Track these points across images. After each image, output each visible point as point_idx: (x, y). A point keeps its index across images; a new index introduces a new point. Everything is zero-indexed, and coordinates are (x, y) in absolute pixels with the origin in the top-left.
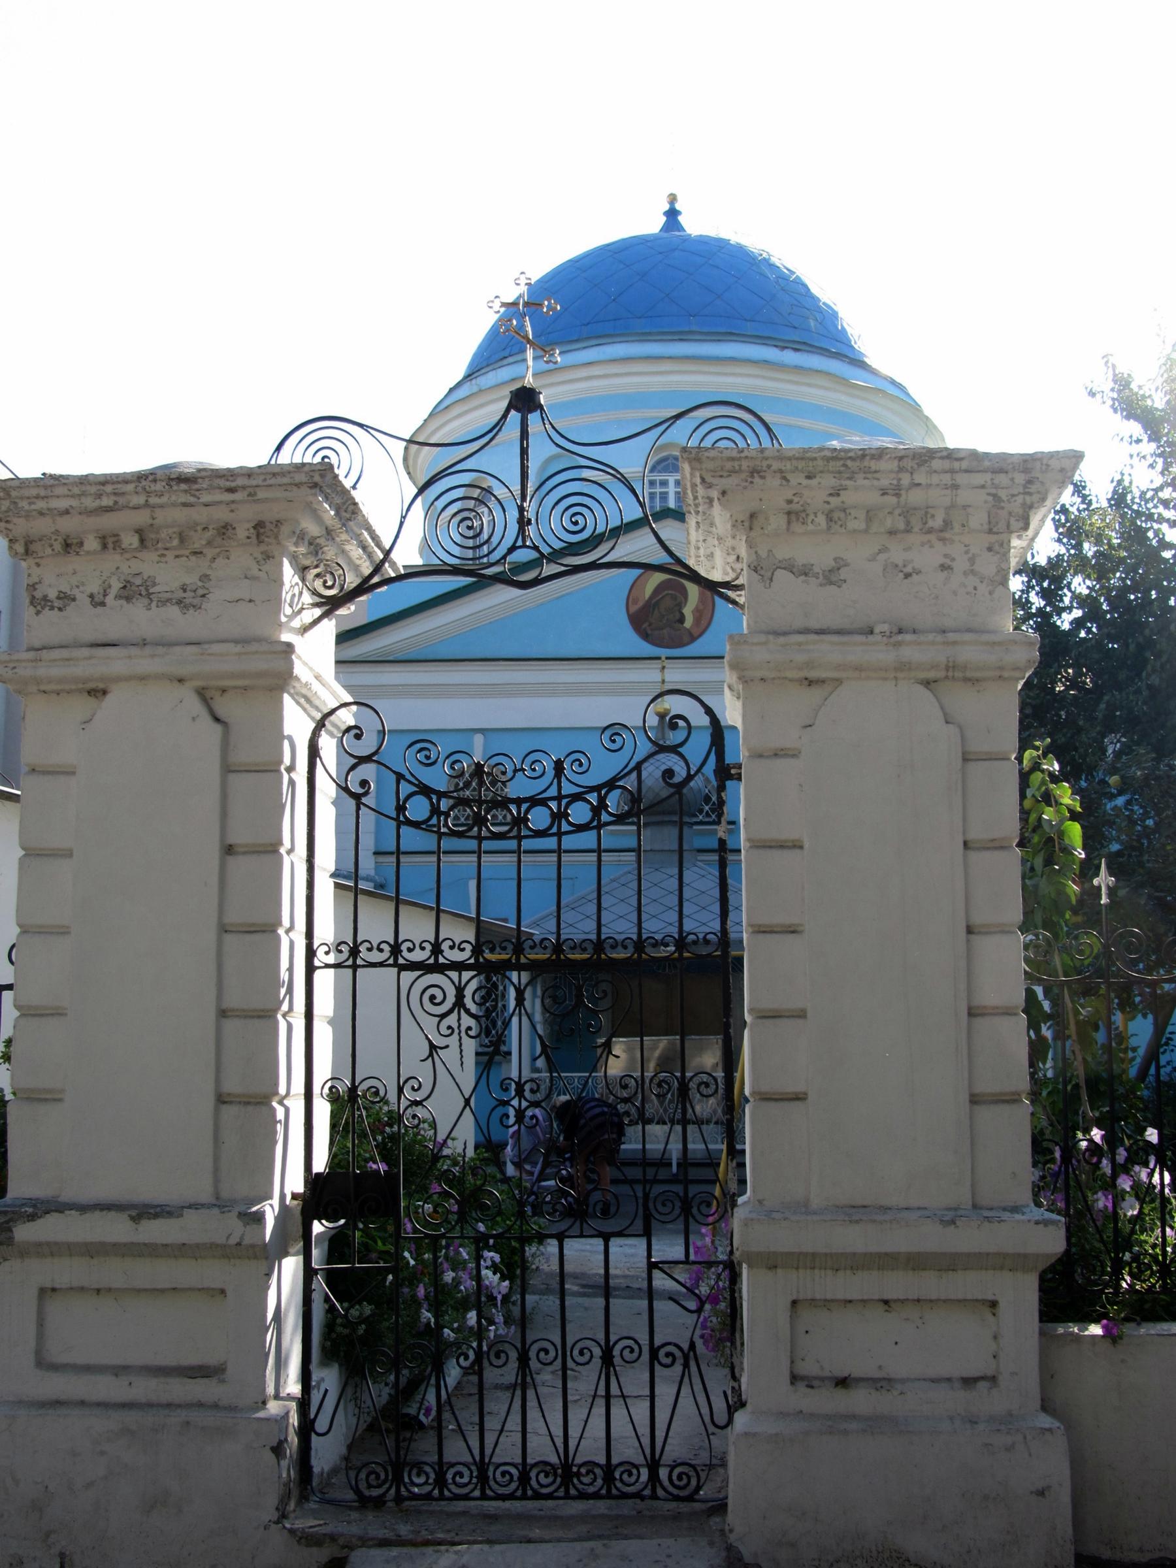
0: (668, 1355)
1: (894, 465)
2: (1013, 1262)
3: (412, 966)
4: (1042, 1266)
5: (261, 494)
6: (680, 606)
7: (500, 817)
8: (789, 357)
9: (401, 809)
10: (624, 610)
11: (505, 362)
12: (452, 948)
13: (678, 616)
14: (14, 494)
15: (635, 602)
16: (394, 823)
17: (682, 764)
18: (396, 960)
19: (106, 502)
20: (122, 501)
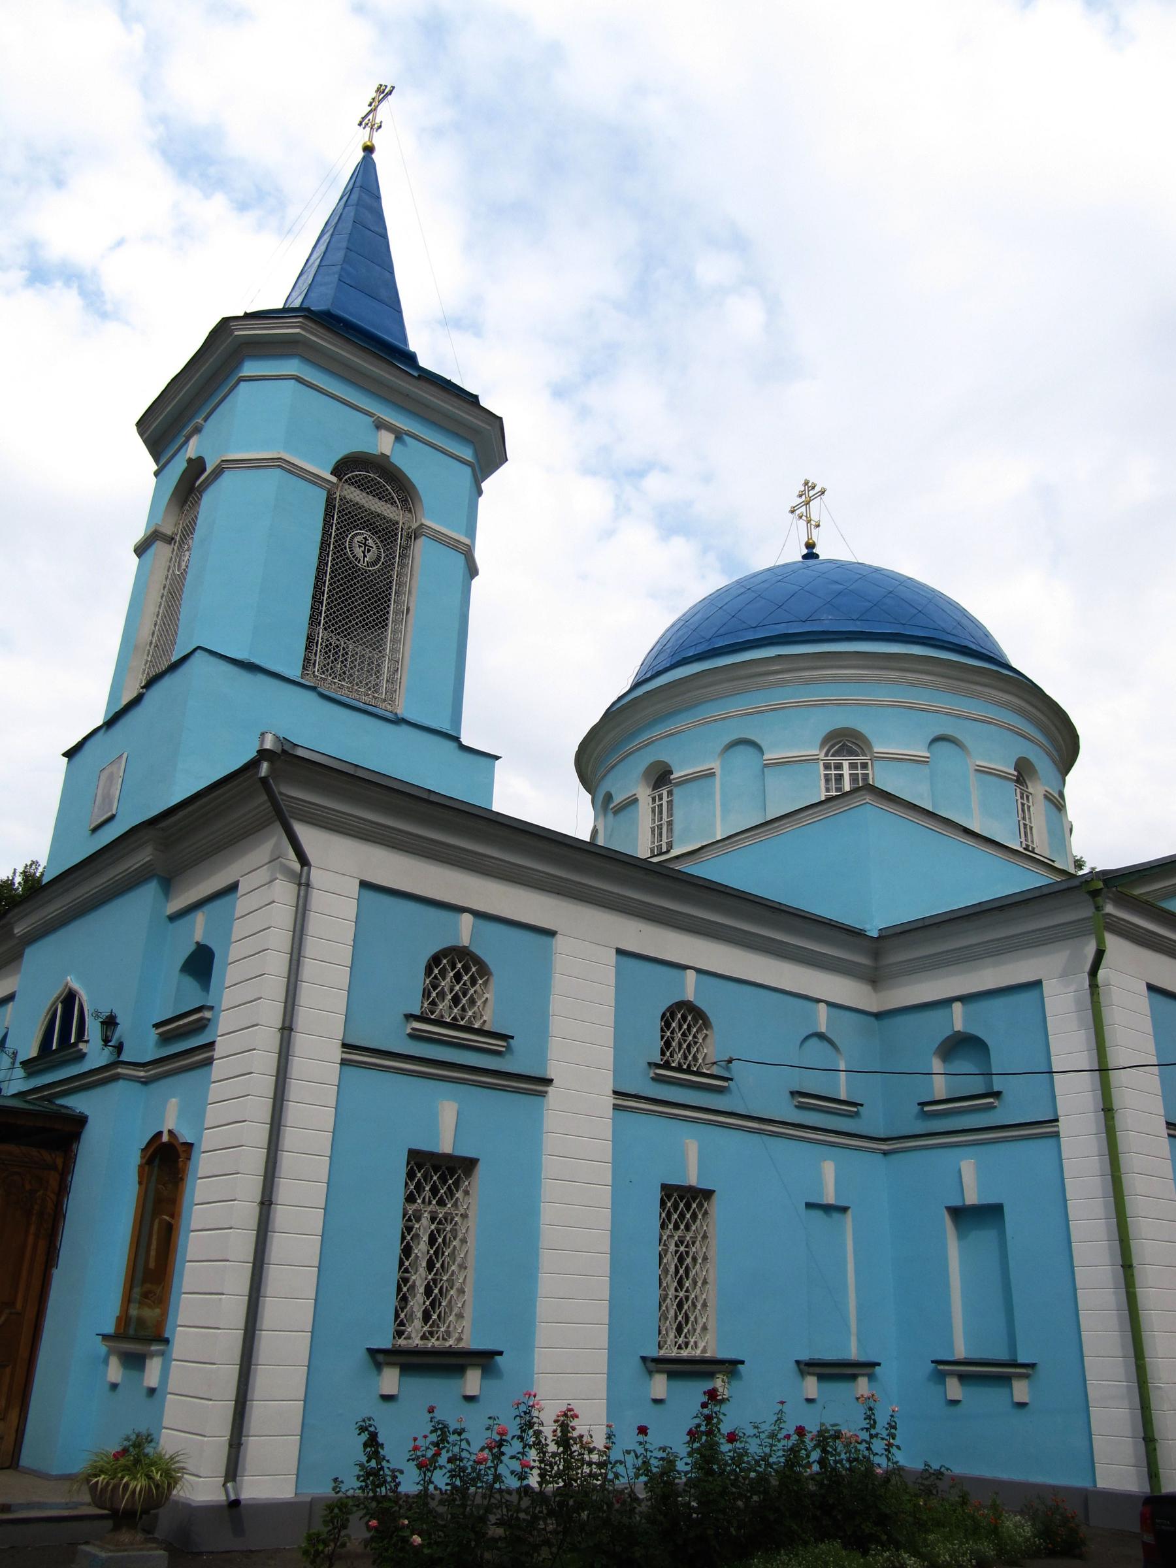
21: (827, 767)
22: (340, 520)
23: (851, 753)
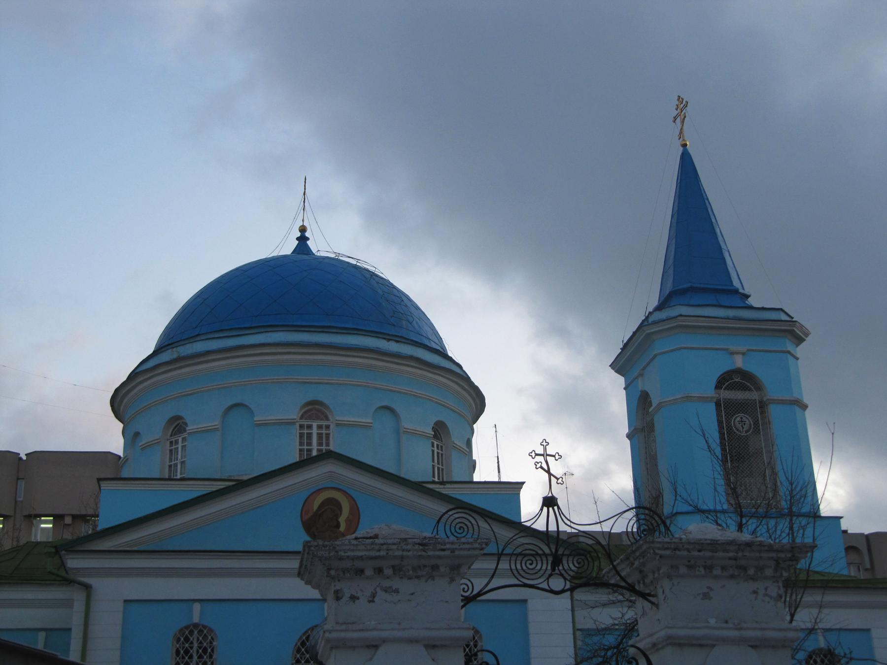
5: (457, 552)
6: (337, 516)
8: (393, 347)
10: (299, 518)
11: (198, 338)
14: (338, 548)
17: (493, 658)
19: (382, 553)
20: (390, 553)
21: (301, 427)
22: (726, 410)
23: (318, 418)
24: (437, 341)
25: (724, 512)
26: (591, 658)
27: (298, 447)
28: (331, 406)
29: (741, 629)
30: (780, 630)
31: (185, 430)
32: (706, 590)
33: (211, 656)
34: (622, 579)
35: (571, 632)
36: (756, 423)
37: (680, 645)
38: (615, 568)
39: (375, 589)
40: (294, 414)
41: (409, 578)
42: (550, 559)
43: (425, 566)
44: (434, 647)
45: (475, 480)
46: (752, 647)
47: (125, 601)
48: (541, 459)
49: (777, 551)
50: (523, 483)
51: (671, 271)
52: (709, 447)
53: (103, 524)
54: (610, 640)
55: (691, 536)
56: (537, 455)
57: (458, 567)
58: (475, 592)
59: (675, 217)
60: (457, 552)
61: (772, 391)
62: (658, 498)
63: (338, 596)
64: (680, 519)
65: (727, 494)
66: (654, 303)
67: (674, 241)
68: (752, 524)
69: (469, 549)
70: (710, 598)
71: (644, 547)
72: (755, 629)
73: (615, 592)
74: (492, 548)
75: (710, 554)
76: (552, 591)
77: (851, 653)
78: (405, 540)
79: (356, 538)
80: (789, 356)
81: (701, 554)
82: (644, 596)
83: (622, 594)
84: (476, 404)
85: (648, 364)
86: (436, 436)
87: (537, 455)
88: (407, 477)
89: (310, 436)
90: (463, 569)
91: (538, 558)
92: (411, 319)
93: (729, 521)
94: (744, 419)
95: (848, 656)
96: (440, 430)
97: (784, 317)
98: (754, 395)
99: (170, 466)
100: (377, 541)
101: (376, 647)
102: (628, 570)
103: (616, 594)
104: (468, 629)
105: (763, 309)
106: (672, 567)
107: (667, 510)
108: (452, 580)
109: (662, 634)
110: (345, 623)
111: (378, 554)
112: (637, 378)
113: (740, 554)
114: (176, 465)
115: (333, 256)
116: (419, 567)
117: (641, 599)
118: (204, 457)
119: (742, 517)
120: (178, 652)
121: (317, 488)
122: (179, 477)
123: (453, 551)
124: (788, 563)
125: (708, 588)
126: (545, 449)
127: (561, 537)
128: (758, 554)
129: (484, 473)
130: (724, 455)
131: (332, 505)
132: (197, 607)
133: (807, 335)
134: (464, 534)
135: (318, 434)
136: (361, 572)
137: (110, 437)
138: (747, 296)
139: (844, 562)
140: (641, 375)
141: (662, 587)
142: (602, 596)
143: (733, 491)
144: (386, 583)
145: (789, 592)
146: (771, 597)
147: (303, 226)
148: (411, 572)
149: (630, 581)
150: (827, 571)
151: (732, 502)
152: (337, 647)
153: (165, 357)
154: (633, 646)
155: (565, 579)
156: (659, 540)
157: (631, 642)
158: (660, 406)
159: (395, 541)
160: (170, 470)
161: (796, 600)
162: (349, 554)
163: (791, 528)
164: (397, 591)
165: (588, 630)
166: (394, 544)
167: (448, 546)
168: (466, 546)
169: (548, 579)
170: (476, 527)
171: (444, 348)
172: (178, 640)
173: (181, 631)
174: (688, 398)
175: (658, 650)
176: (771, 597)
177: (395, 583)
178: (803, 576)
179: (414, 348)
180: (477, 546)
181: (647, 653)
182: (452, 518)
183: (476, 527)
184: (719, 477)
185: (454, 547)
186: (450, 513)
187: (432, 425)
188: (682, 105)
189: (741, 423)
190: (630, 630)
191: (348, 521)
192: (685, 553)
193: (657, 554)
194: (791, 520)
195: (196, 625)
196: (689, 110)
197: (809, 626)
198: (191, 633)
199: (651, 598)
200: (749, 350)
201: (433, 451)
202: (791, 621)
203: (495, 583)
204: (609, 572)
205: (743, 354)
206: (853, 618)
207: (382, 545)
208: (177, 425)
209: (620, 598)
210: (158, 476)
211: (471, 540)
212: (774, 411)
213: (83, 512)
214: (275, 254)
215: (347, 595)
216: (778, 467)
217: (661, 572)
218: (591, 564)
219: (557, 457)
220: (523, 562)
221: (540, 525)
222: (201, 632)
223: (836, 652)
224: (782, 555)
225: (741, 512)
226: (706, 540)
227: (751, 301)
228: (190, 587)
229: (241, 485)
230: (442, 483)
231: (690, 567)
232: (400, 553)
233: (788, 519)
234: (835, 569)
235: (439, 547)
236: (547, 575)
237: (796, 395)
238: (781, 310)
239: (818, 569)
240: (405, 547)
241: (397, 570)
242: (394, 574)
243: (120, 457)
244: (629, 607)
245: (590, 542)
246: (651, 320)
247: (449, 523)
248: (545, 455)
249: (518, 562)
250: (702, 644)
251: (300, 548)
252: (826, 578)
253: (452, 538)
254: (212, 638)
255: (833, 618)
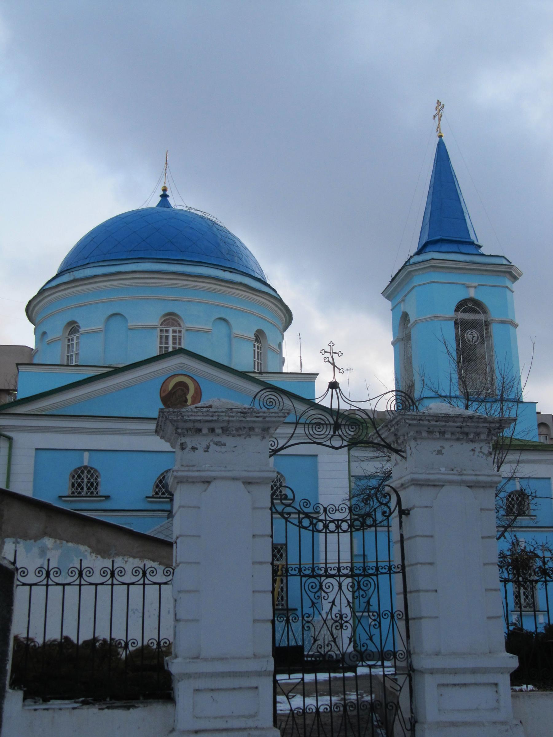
0: (391, 706)
1: (462, 420)
2: (500, 671)
3: (305, 576)
4: (511, 671)
5: (267, 419)
7: (95, 493)
8: (228, 276)
9: (300, 522)
11: (88, 266)
12: (331, 570)
13: (184, 399)
14: (183, 414)
15: (164, 391)
16: (298, 528)
17: (290, 491)
18: (300, 574)
19: (215, 418)
21: (161, 331)
22: (461, 326)
23: (173, 325)
24: (259, 273)
25: (456, 397)
26: (360, 495)
27: (159, 345)
28: (182, 317)
29: (462, 475)
30: (489, 476)
31: (78, 331)
32: (440, 448)
33: (96, 489)
34: (383, 440)
35: (348, 477)
36: (482, 336)
37: (421, 485)
38: (377, 432)
39: (209, 443)
40: (156, 322)
41: (233, 436)
42: (332, 426)
43: (244, 428)
44: (250, 483)
45: (284, 371)
46: (469, 487)
47: (37, 449)
48: (328, 355)
49: (490, 422)
50: (317, 374)
51: (427, 227)
52: (448, 351)
53: (20, 395)
54: (374, 483)
55: (431, 412)
56: (326, 352)
57: (268, 428)
58: (279, 447)
59: (432, 188)
60: (267, 419)
61: (494, 314)
62: (411, 387)
63: (183, 447)
64: (426, 402)
65: (459, 384)
66: (415, 250)
67: (430, 206)
68: (475, 405)
69: (276, 417)
70: (442, 454)
71: (398, 418)
72: (471, 475)
73: (378, 450)
74: (291, 418)
75: (443, 423)
76: (333, 447)
77: (535, 492)
78: (231, 409)
79: (196, 407)
80: (507, 290)
81: (438, 423)
82: (397, 452)
83: (383, 452)
84: (286, 318)
85: (408, 293)
86: (257, 340)
87: (326, 352)
88: (236, 368)
89: (167, 337)
90: (272, 431)
91: (325, 427)
92: (241, 256)
93: (460, 403)
94: (474, 333)
95: (533, 495)
96: (259, 336)
97: (505, 262)
98: (481, 317)
99: (68, 356)
100: (211, 410)
101: (209, 482)
102: (387, 433)
103: (379, 452)
104: (274, 471)
105: (491, 256)
106: (417, 432)
107: (417, 395)
108: (263, 438)
109: (409, 477)
110: (187, 466)
111: (211, 418)
112: (400, 302)
113: (464, 424)
114: (72, 356)
115: (186, 209)
116: (240, 428)
117: (395, 453)
118: (93, 351)
119: (468, 400)
120: (73, 485)
121: (172, 374)
122: (74, 364)
123: (264, 418)
124: (496, 431)
125: (441, 447)
126: (332, 349)
127: (340, 411)
128: (476, 424)
129: (290, 366)
130: (459, 359)
131: (182, 387)
132: (86, 454)
133: (520, 276)
134: (274, 405)
135: (173, 336)
136: (199, 431)
137: (24, 335)
138: (480, 247)
139: (536, 432)
140: (403, 300)
141: (409, 445)
142: (370, 453)
143: (463, 382)
144: (217, 439)
145: (498, 452)
146: (483, 453)
147: (165, 187)
148: (234, 432)
149: (387, 441)
150: (524, 438)
151: (462, 390)
152: (181, 482)
153: (65, 278)
154: (387, 485)
155: (343, 439)
156: (409, 413)
157: (386, 483)
158: (416, 323)
159: (224, 410)
160: (68, 359)
161: (502, 457)
162: (191, 418)
163: (502, 409)
164: (224, 445)
165: (359, 476)
166: (223, 412)
167: (261, 414)
168: (274, 415)
169: (330, 439)
170: (281, 403)
171: (264, 278)
172: (73, 477)
173: (76, 471)
174: (435, 318)
175: (405, 488)
176: (483, 453)
177: (224, 439)
178: (507, 442)
179: (249, 284)
180: (281, 414)
181: (397, 490)
182: (263, 396)
183: (281, 403)
184: (454, 372)
185: (265, 415)
186: (262, 393)
187: (254, 332)
188: (440, 106)
189: (472, 335)
190: (387, 477)
191: (193, 397)
192: (426, 423)
193: (407, 423)
194: (502, 403)
195: (86, 467)
196: (445, 112)
197: (510, 476)
198: (82, 472)
199: (401, 453)
200: (479, 285)
201: (254, 351)
202: (498, 471)
203: (292, 442)
204: (373, 435)
205: (475, 287)
206: (540, 471)
207: (215, 412)
208: (73, 328)
209: (382, 454)
210: (59, 363)
211: (277, 411)
212: (495, 329)
213: (7, 388)
214: (144, 206)
215: (189, 447)
216: (495, 366)
217: (409, 435)
218: (361, 431)
219: (340, 354)
220: (314, 429)
221: (326, 403)
222: (89, 472)
223: (526, 492)
224: (493, 425)
225: (468, 397)
226: (441, 414)
227: (482, 250)
228: (82, 441)
229: (117, 371)
230: (260, 373)
231: (429, 432)
232: (227, 418)
233: (500, 403)
234: (528, 438)
235: (255, 414)
236: (329, 436)
237: (510, 318)
238: (503, 257)
239: (517, 437)
240: (231, 414)
241: (225, 430)
242: (223, 432)
243: (33, 349)
244: (388, 461)
245: (365, 416)
246: (412, 261)
247: (261, 400)
248: (331, 353)
249: (310, 429)
250: (435, 485)
251: (155, 415)
252: (523, 444)
253: (264, 409)
254: (97, 476)
255: (525, 470)
